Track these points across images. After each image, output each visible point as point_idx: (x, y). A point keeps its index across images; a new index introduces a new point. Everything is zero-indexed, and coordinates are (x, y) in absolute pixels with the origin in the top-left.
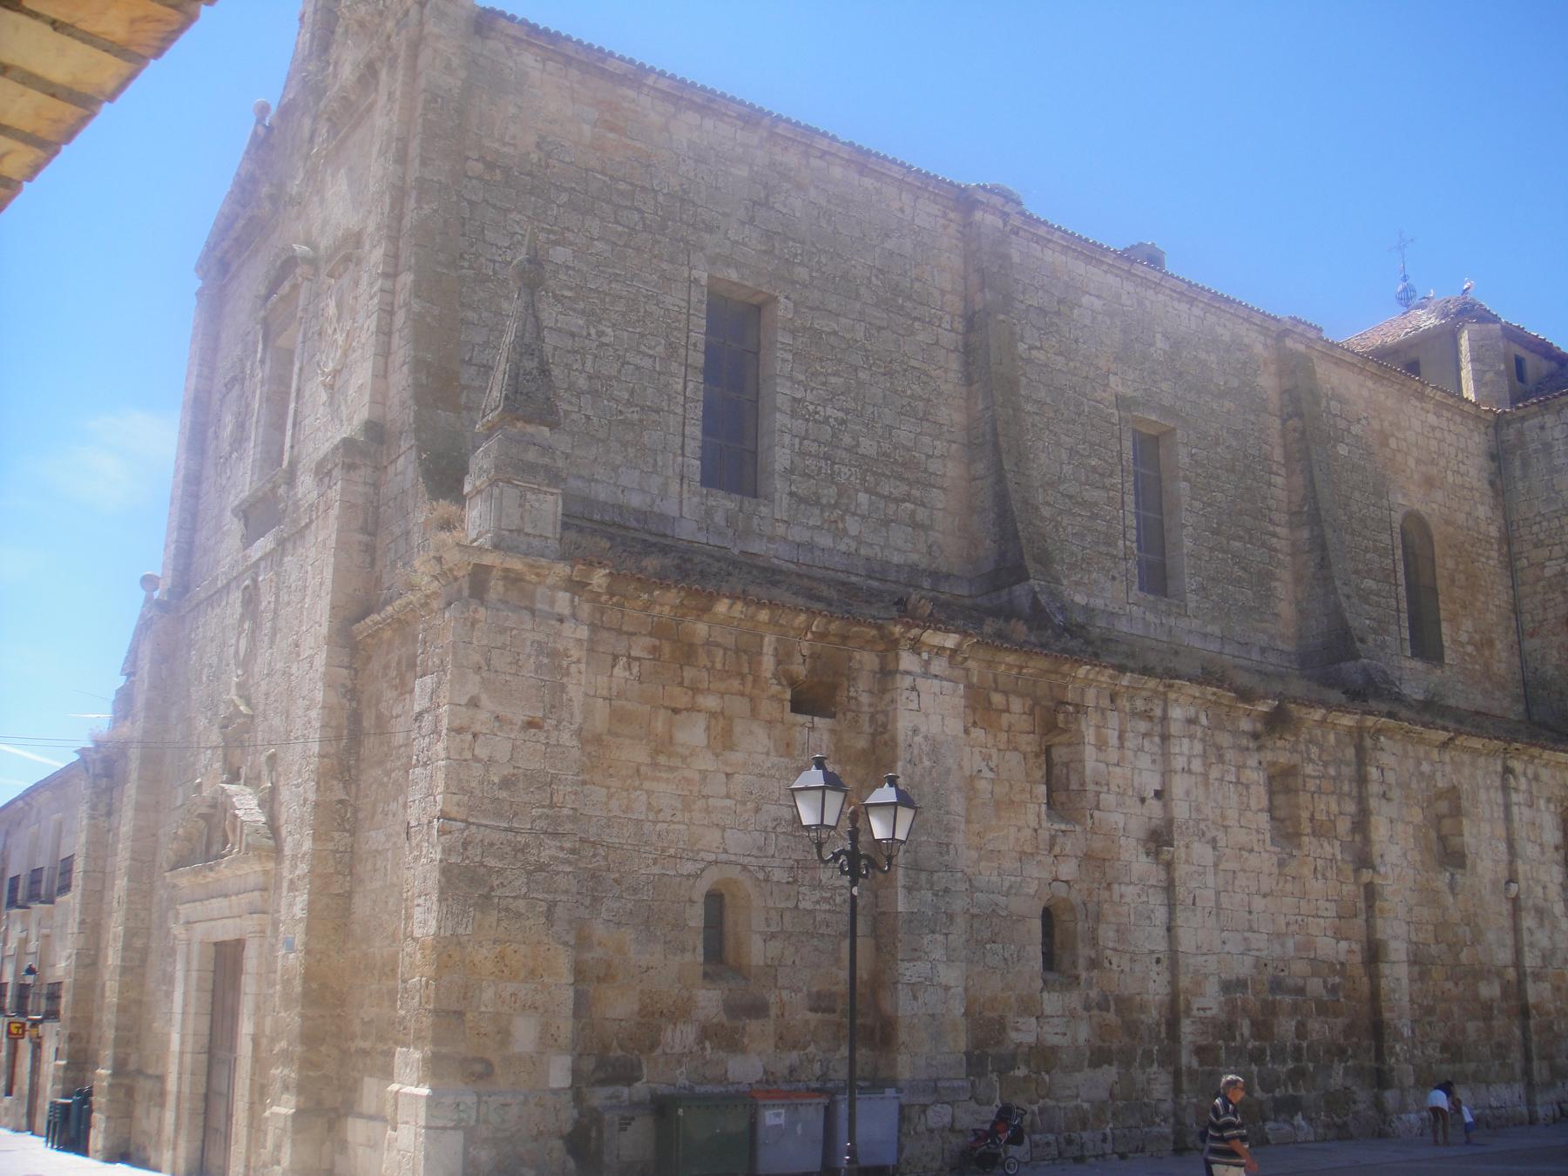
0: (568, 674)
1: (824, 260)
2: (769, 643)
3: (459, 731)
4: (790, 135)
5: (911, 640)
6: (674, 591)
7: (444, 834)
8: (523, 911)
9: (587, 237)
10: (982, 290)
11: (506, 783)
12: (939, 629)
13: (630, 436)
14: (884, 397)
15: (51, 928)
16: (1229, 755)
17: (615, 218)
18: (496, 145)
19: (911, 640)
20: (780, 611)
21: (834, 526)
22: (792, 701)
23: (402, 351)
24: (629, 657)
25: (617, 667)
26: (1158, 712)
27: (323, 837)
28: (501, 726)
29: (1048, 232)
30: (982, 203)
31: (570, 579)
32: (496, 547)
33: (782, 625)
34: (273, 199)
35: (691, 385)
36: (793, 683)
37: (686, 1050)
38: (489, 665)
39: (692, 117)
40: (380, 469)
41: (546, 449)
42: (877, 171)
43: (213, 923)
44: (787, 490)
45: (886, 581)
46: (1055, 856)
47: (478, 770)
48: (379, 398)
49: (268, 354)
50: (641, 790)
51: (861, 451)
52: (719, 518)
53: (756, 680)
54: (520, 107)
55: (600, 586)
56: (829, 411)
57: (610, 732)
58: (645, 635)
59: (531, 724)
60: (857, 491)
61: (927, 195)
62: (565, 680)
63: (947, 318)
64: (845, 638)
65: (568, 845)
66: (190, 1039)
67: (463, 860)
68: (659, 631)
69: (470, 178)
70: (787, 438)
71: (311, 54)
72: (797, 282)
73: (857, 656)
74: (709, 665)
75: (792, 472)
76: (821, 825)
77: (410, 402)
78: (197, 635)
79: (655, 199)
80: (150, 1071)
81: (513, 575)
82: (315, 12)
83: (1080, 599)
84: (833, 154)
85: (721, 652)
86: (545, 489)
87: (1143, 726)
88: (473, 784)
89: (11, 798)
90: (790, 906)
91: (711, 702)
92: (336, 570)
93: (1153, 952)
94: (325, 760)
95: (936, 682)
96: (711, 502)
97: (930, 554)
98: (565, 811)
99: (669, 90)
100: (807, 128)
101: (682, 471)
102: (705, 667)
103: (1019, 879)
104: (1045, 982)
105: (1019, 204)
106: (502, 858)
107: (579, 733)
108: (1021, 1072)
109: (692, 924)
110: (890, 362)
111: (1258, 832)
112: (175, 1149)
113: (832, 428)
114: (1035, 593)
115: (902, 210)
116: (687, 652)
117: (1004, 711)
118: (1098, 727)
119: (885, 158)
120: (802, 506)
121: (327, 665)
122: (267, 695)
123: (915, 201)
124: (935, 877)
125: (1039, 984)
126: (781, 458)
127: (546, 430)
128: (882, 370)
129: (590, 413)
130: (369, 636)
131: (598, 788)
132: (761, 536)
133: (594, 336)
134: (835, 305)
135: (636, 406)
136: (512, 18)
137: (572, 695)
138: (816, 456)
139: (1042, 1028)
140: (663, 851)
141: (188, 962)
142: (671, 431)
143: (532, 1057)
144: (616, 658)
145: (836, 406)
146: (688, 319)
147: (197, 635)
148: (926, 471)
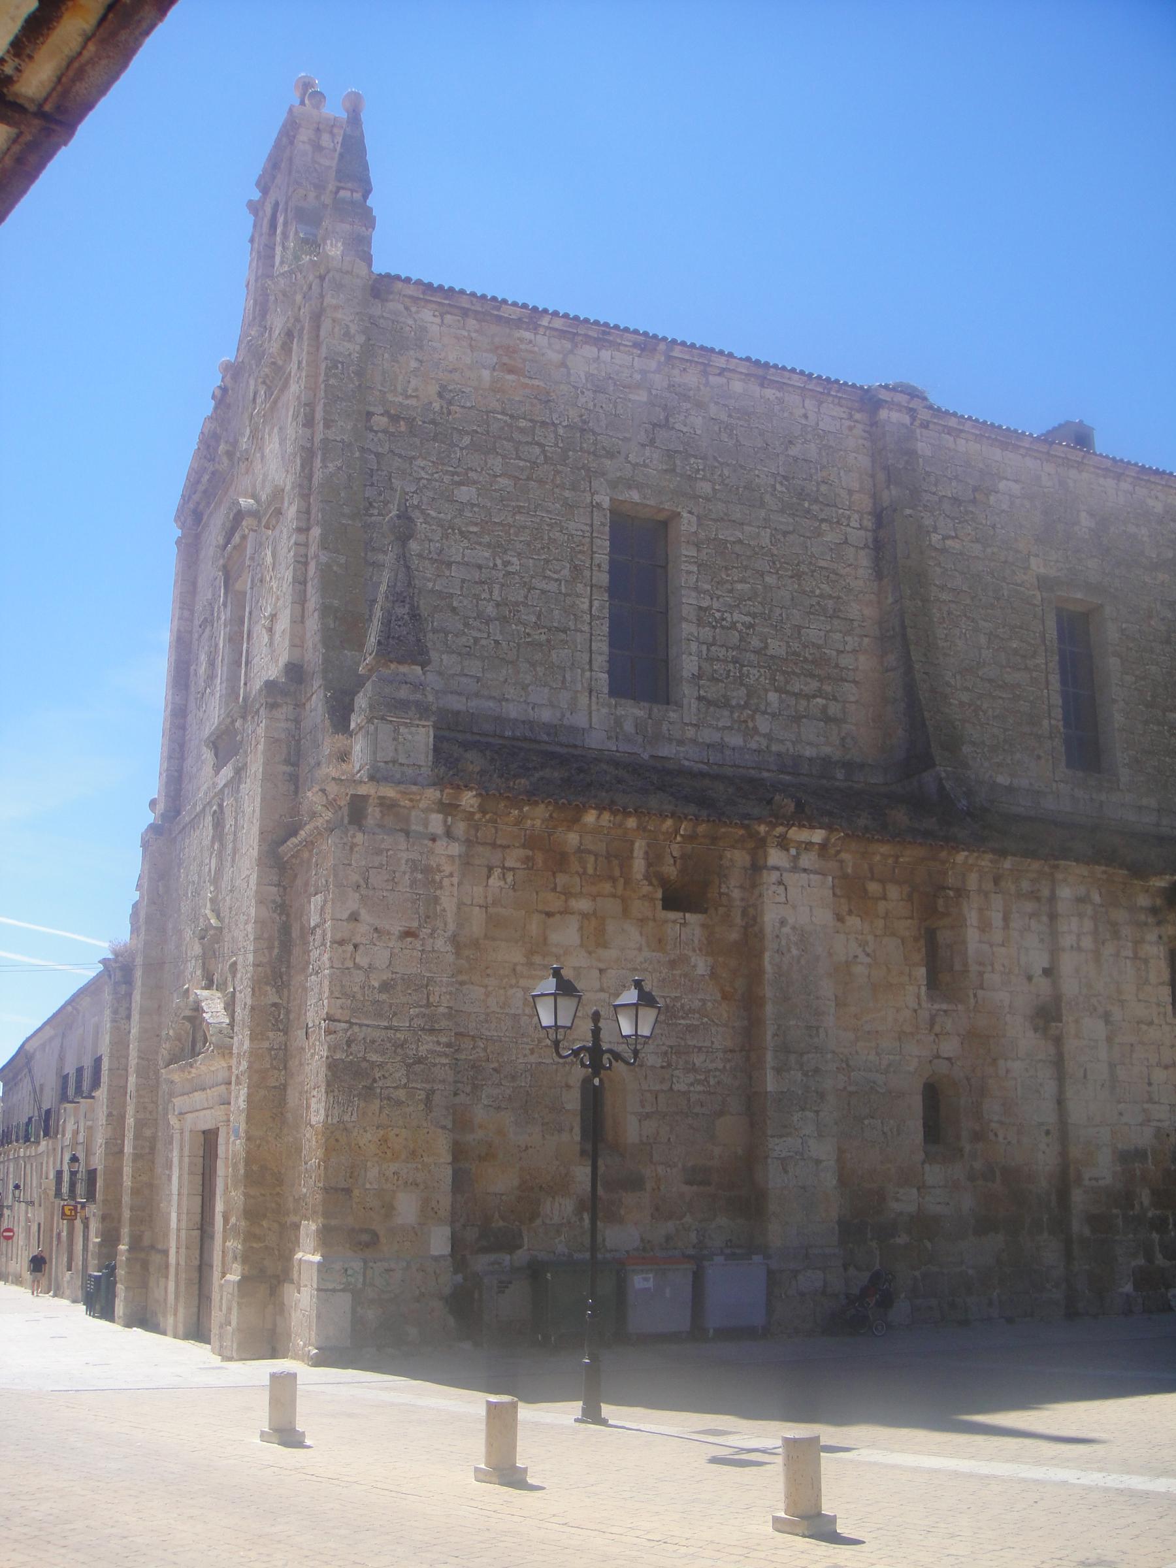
0: (441, 888)
1: (726, 473)
2: (639, 847)
3: (341, 943)
4: (687, 357)
5: (778, 837)
6: (542, 806)
7: (330, 1034)
8: (404, 1099)
9: (489, 474)
10: (888, 487)
11: (386, 987)
12: (804, 826)
13: (538, 656)
14: (792, 599)
15: (93, 1120)
16: (1126, 931)
17: (517, 453)
18: (400, 399)
19: (778, 837)
20: (647, 818)
21: (744, 726)
22: (664, 899)
23: (313, 600)
24: (503, 868)
25: (492, 877)
26: (1046, 893)
27: (259, 1037)
28: (379, 937)
29: (959, 423)
30: (886, 402)
31: (440, 802)
32: (372, 778)
33: (650, 831)
34: (230, 454)
35: (596, 604)
36: (664, 882)
37: (565, 1220)
38: (367, 884)
39: (589, 351)
40: (299, 705)
41: (418, 686)
42: (777, 382)
43: (197, 1113)
44: (696, 694)
45: (799, 774)
46: (936, 1035)
47: (359, 977)
48: (297, 642)
49: (229, 596)
50: (518, 987)
51: (770, 652)
52: (629, 727)
53: (627, 882)
54: (421, 362)
55: (472, 806)
56: (736, 617)
57: (486, 937)
58: (518, 847)
59: (408, 934)
60: (766, 691)
61: (831, 399)
62: (438, 893)
63: (856, 516)
64: (714, 839)
65: (444, 1040)
66: (184, 1217)
67: (347, 1056)
68: (531, 842)
69: (376, 432)
70: (694, 646)
71: (254, 319)
72: (700, 497)
73: (728, 854)
74: (581, 870)
75: (700, 677)
76: (556, 1027)
77: (319, 646)
78: (184, 855)
79: (555, 432)
80: (160, 1247)
81: (388, 802)
82: (256, 281)
83: (1003, 779)
84: (730, 370)
85: (592, 859)
86: (417, 722)
87: (1029, 906)
88: (355, 989)
89: (60, 1006)
90: (664, 1088)
91: (584, 905)
92: (263, 799)
93: (1042, 1124)
94: (260, 968)
95: (804, 875)
96: (620, 711)
97: (844, 746)
98: (441, 1010)
99: (565, 329)
100: (702, 348)
101: (590, 684)
102: (577, 873)
103: (898, 1057)
104: (926, 1153)
105: (925, 399)
106: (383, 1054)
107: (454, 940)
108: (902, 1239)
109: (568, 1107)
110: (798, 565)
111: (1158, 1005)
112: (175, 1314)
113: (740, 632)
114: (941, 779)
115: (806, 416)
116: (559, 860)
117: (880, 899)
118: (981, 910)
119: (784, 368)
120: (712, 709)
121: (258, 884)
122: (230, 908)
123: (819, 406)
124: (805, 1057)
125: (920, 1156)
126: (689, 665)
127: (418, 669)
128: (789, 573)
129: (499, 637)
130: (293, 856)
131: (477, 988)
132: (670, 740)
133: (500, 566)
134: (739, 515)
135: (544, 627)
136: (408, 280)
137: (445, 906)
138: (725, 661)
139: (923, 1198)
140: (540, 1041)
141: (182, 1149)
142: (579, 647)
143: (414, 1228)
144: (490, 869)
145: (743, 612)
146: (592, 543)
147: (184, 855)
148: (837, 666)
